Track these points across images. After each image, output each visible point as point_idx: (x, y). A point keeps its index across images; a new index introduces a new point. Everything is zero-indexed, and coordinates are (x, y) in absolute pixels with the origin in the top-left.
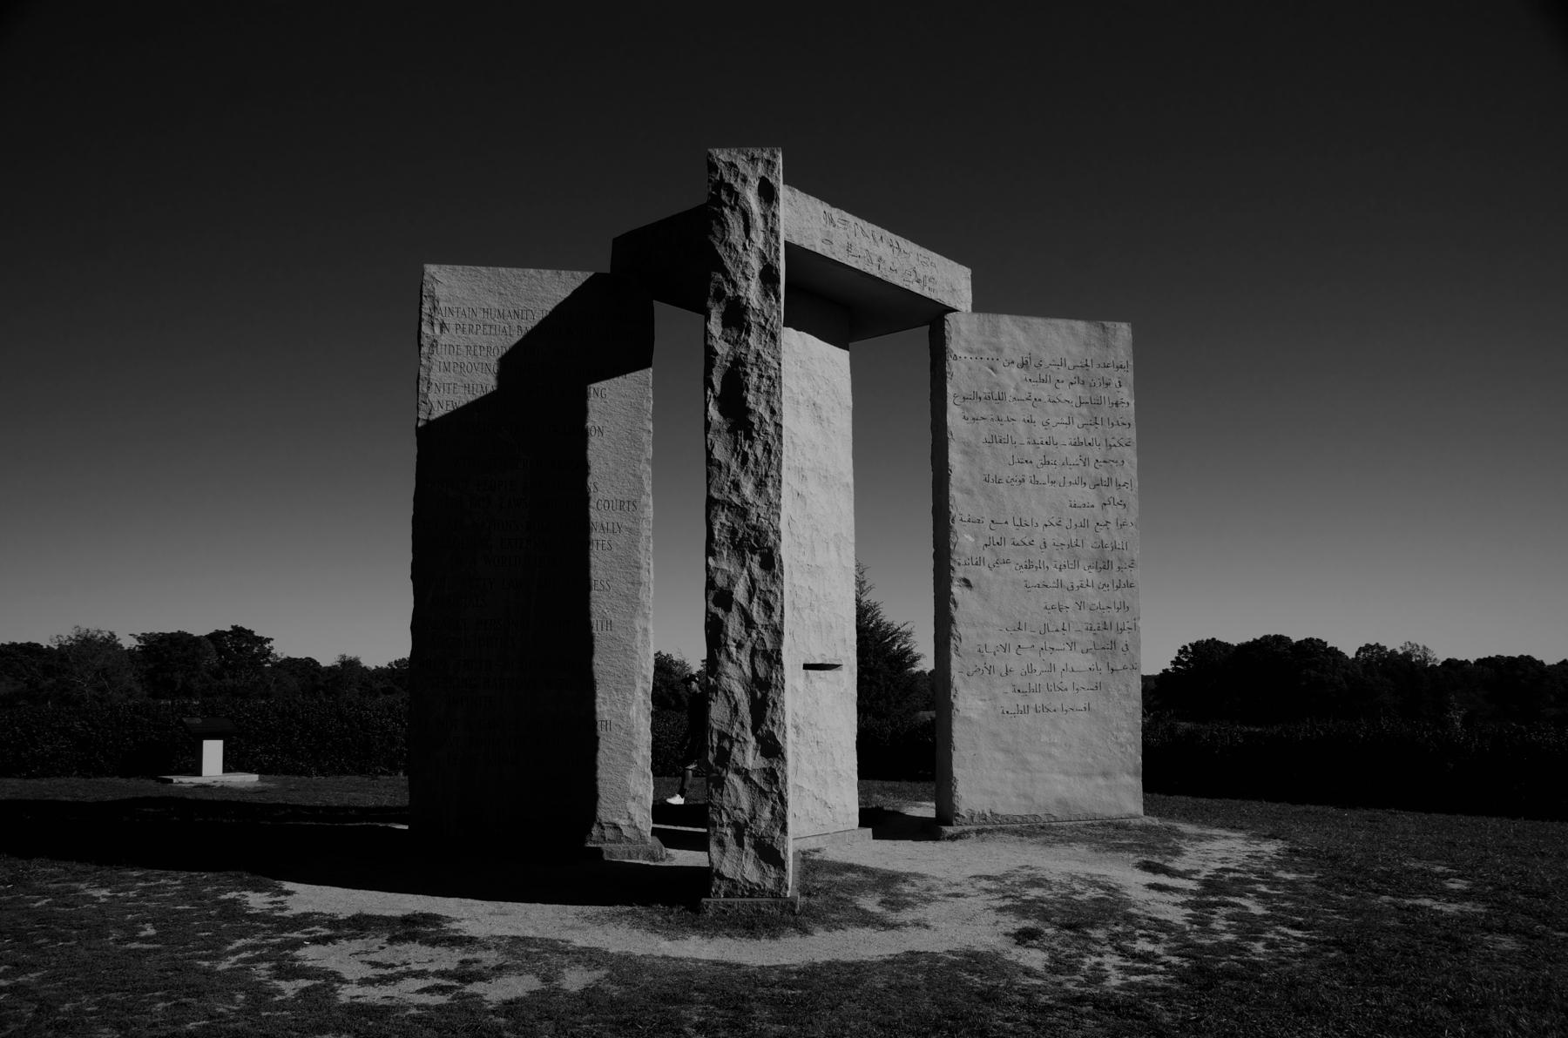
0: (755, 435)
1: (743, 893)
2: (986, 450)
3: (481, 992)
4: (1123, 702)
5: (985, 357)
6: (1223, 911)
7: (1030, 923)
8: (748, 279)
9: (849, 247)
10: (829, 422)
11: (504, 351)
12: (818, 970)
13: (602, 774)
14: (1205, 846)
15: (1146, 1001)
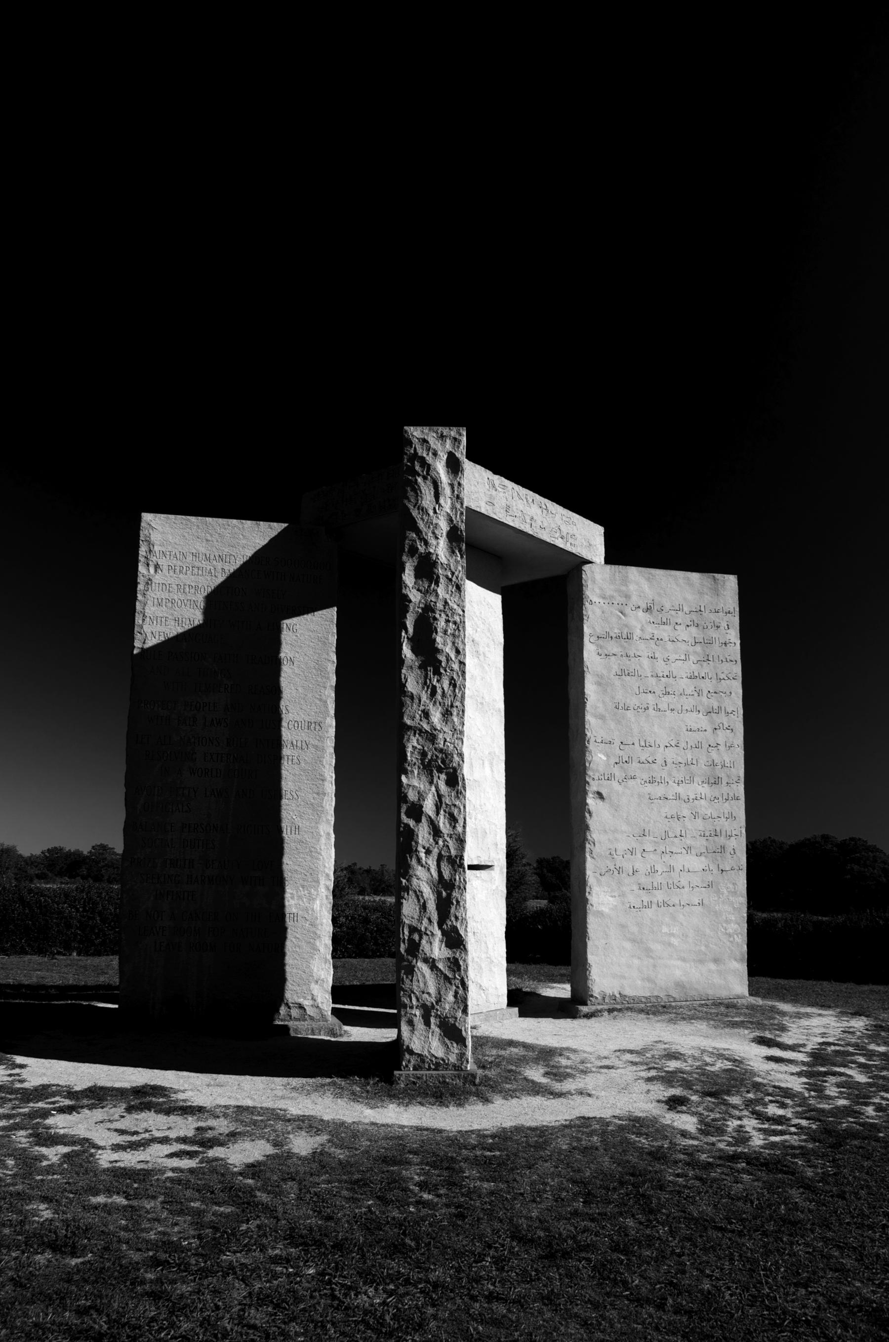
0: (442, 671)
1: (429, 1066)
2: (617, 682)
3: (223, 1156)
4: (731, 898)
5: (615, 603)
6: (832, 1079)
7: (677, 1091)
8: (437, 538)
9: (508, 509)
10: (485, 656)
11: (210, 590)
12: (509, 1133)
13: (289, 960)
14: (804, 1022)
15: (788, 1158)
